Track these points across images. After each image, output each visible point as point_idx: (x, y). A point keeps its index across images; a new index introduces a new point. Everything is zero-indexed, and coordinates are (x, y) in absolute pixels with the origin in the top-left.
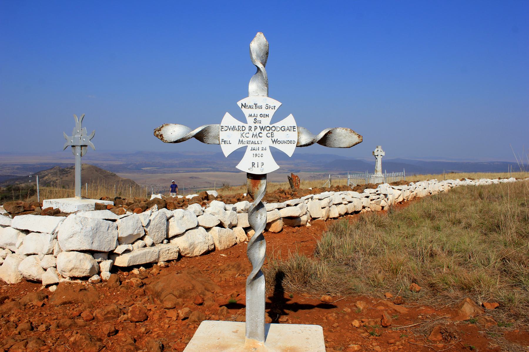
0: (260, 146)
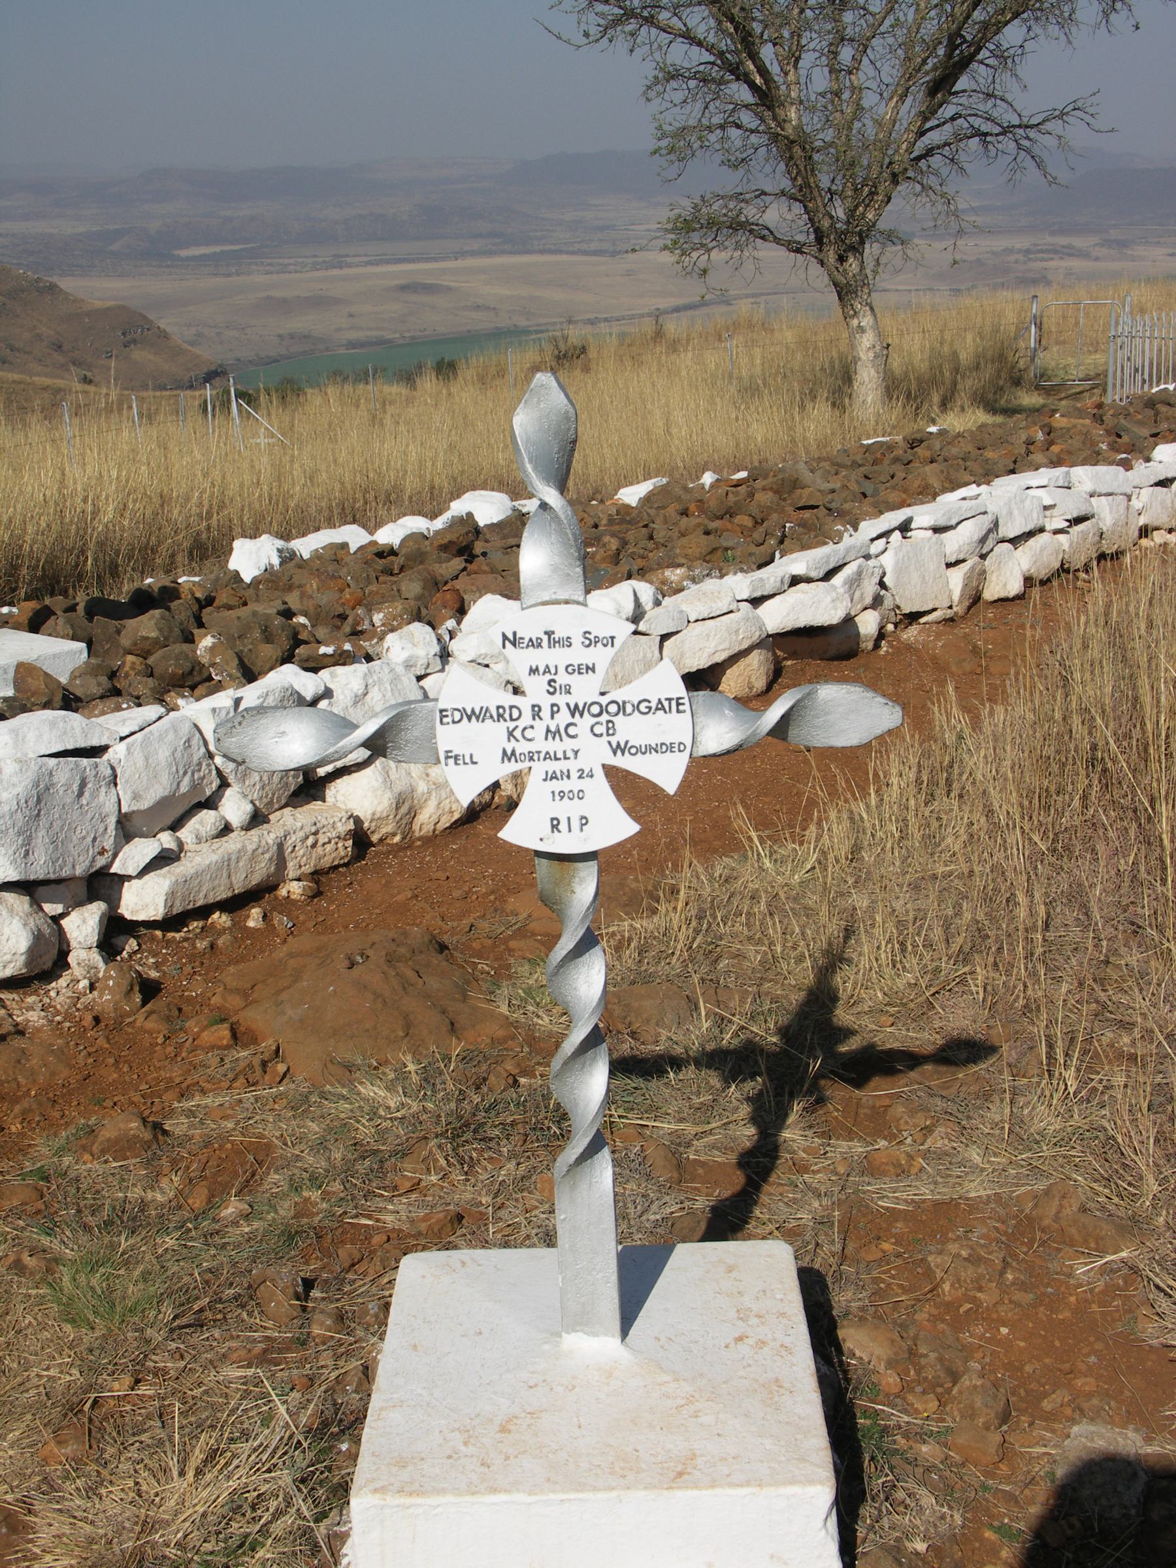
0: (573, 765)
